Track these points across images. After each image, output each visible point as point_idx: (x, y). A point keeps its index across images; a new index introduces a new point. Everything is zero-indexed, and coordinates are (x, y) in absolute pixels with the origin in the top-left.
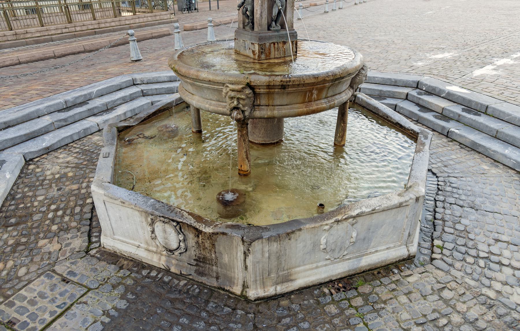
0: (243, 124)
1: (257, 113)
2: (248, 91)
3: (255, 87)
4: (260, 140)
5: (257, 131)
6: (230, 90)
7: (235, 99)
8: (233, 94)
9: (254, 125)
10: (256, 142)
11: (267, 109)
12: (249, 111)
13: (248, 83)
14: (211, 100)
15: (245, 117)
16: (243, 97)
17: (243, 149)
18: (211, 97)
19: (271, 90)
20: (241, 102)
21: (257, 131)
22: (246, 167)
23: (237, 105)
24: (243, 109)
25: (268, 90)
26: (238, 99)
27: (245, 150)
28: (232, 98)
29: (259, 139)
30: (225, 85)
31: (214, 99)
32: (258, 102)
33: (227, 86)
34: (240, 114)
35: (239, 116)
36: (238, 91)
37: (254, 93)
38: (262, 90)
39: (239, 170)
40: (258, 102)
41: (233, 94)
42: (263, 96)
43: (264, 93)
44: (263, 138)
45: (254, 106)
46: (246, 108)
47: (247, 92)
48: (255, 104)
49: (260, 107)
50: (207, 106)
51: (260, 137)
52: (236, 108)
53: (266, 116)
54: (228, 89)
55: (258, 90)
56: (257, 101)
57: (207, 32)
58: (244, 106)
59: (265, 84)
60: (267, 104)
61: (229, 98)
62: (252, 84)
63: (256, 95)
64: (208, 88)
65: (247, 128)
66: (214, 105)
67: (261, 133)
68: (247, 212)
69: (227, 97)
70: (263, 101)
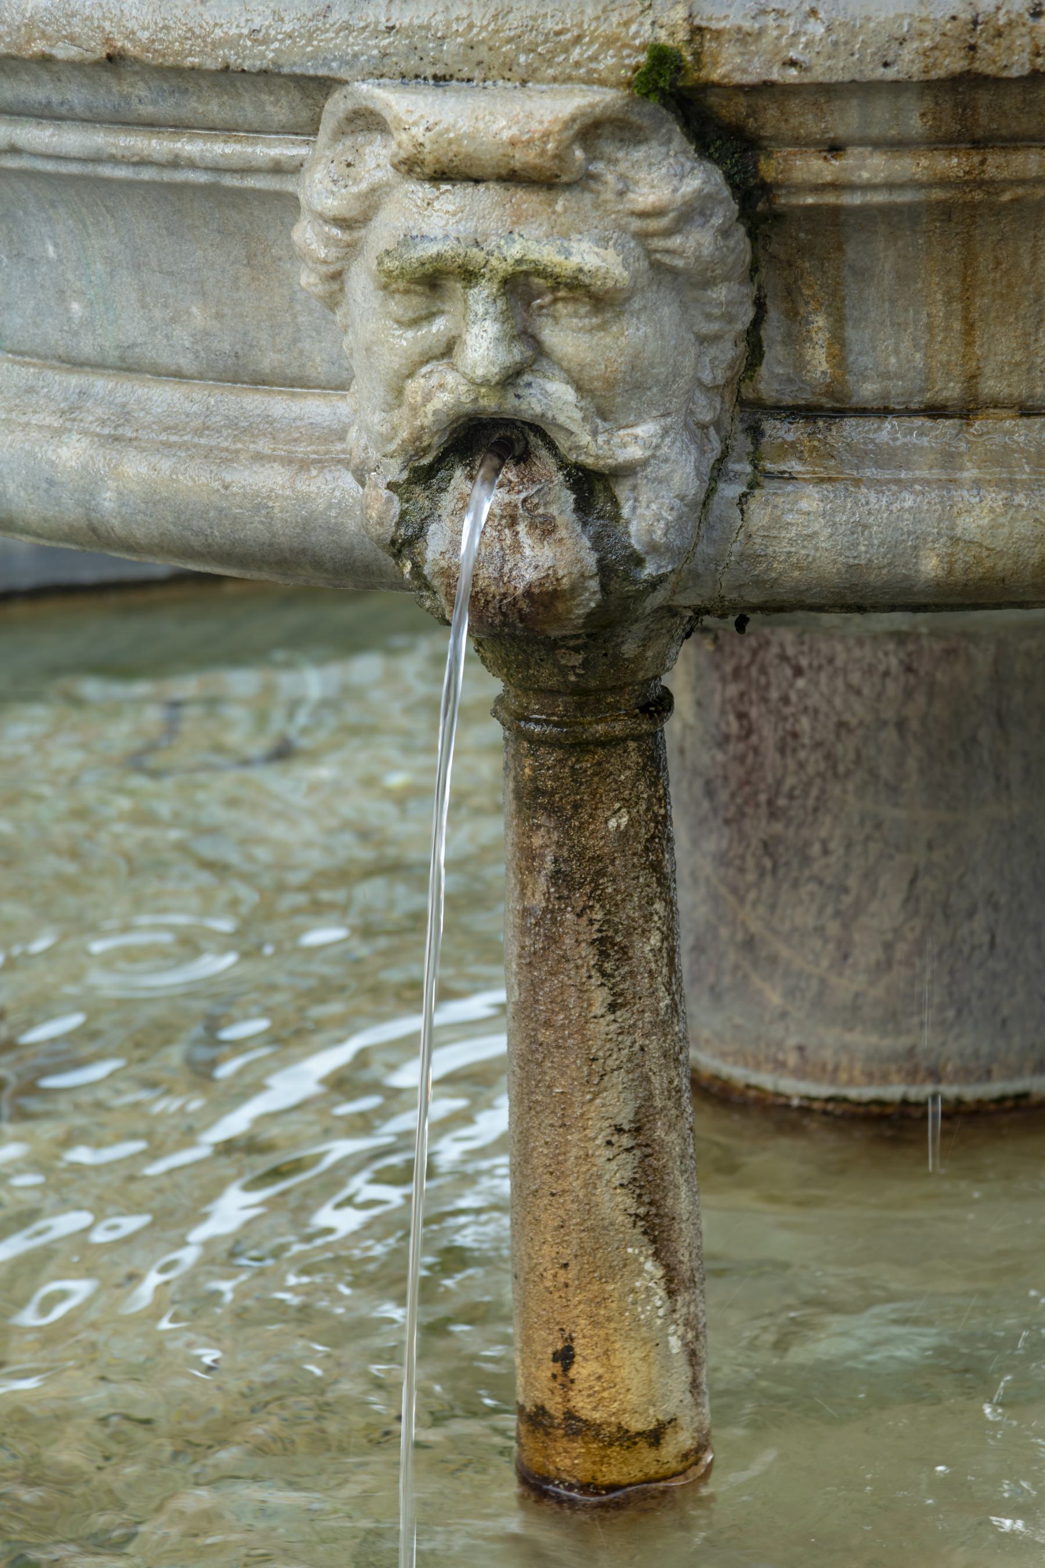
0: (585, 698)
1: (807, 522)
2: (663, 177)
3: (769, 119)
4: (840, 1057)
5: (804, 917)
6: (410, 166)
7: (481, 298)
8: (442, 221)
9: (759, 828)
10: (794, 1088)
11: (949, 459)
12: (683, 473)
13: (661, 58)
14: (128, 366)
15: (615, 566)
16: (589, 256)
17: (596, 1081)
18: (130, 328)
19: (998, 165)
20: (566, 336)
21: (804, 917)
22: (631, 1378)
23: (511, 378)
24: (592, 446)
25: (952, 164)
26: (524, 291)
27: (617, 1104)
28: (433, 282)
29: (829, 1040)
30: (336, 107)
31: (176, 346)
32: (819, 361)
33: (367, 121)
34: (546, 529)
35: (535, 560)
36: (512, 178)
37: (756, 205)
38: (870, 166)
39: (536, 1419)
40: (819, 361)
41: (442, 221)
42: (885, 257)
43: (890, 218)
44: (890, 1020)
45: (757, 417)
46: (634, 441)
47: (645, 197)
48: (770, 382)
49: (851, 428)
50: (71, 453)
51: (852, 1014)
52: (486, 438)
53: (930, 565)
54: (376, 159)
55: (813, 167)
56: (796, 339)
57: (426, 1208)
58: (603, 404)
59: (908, 64)
60: (952, 391)
61: (388, 283)
62: (727, 65)
63: (780, 241)
64: (83, 188)
65: (654, 764)
66: (172, 437)
67: (867, 952)
68: (517, 464)
69: (361, 282)
70: (888, 336)
